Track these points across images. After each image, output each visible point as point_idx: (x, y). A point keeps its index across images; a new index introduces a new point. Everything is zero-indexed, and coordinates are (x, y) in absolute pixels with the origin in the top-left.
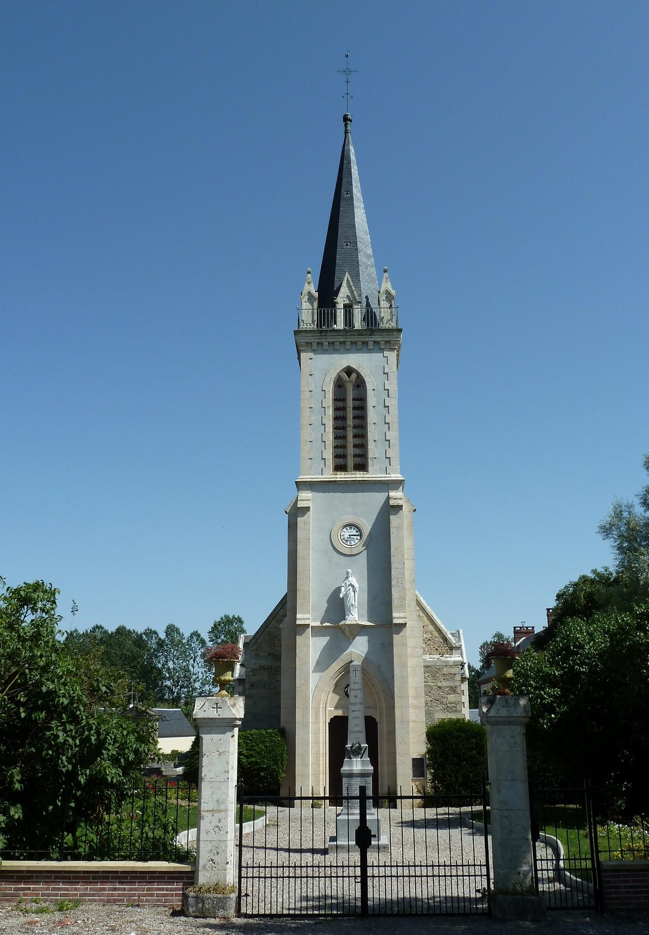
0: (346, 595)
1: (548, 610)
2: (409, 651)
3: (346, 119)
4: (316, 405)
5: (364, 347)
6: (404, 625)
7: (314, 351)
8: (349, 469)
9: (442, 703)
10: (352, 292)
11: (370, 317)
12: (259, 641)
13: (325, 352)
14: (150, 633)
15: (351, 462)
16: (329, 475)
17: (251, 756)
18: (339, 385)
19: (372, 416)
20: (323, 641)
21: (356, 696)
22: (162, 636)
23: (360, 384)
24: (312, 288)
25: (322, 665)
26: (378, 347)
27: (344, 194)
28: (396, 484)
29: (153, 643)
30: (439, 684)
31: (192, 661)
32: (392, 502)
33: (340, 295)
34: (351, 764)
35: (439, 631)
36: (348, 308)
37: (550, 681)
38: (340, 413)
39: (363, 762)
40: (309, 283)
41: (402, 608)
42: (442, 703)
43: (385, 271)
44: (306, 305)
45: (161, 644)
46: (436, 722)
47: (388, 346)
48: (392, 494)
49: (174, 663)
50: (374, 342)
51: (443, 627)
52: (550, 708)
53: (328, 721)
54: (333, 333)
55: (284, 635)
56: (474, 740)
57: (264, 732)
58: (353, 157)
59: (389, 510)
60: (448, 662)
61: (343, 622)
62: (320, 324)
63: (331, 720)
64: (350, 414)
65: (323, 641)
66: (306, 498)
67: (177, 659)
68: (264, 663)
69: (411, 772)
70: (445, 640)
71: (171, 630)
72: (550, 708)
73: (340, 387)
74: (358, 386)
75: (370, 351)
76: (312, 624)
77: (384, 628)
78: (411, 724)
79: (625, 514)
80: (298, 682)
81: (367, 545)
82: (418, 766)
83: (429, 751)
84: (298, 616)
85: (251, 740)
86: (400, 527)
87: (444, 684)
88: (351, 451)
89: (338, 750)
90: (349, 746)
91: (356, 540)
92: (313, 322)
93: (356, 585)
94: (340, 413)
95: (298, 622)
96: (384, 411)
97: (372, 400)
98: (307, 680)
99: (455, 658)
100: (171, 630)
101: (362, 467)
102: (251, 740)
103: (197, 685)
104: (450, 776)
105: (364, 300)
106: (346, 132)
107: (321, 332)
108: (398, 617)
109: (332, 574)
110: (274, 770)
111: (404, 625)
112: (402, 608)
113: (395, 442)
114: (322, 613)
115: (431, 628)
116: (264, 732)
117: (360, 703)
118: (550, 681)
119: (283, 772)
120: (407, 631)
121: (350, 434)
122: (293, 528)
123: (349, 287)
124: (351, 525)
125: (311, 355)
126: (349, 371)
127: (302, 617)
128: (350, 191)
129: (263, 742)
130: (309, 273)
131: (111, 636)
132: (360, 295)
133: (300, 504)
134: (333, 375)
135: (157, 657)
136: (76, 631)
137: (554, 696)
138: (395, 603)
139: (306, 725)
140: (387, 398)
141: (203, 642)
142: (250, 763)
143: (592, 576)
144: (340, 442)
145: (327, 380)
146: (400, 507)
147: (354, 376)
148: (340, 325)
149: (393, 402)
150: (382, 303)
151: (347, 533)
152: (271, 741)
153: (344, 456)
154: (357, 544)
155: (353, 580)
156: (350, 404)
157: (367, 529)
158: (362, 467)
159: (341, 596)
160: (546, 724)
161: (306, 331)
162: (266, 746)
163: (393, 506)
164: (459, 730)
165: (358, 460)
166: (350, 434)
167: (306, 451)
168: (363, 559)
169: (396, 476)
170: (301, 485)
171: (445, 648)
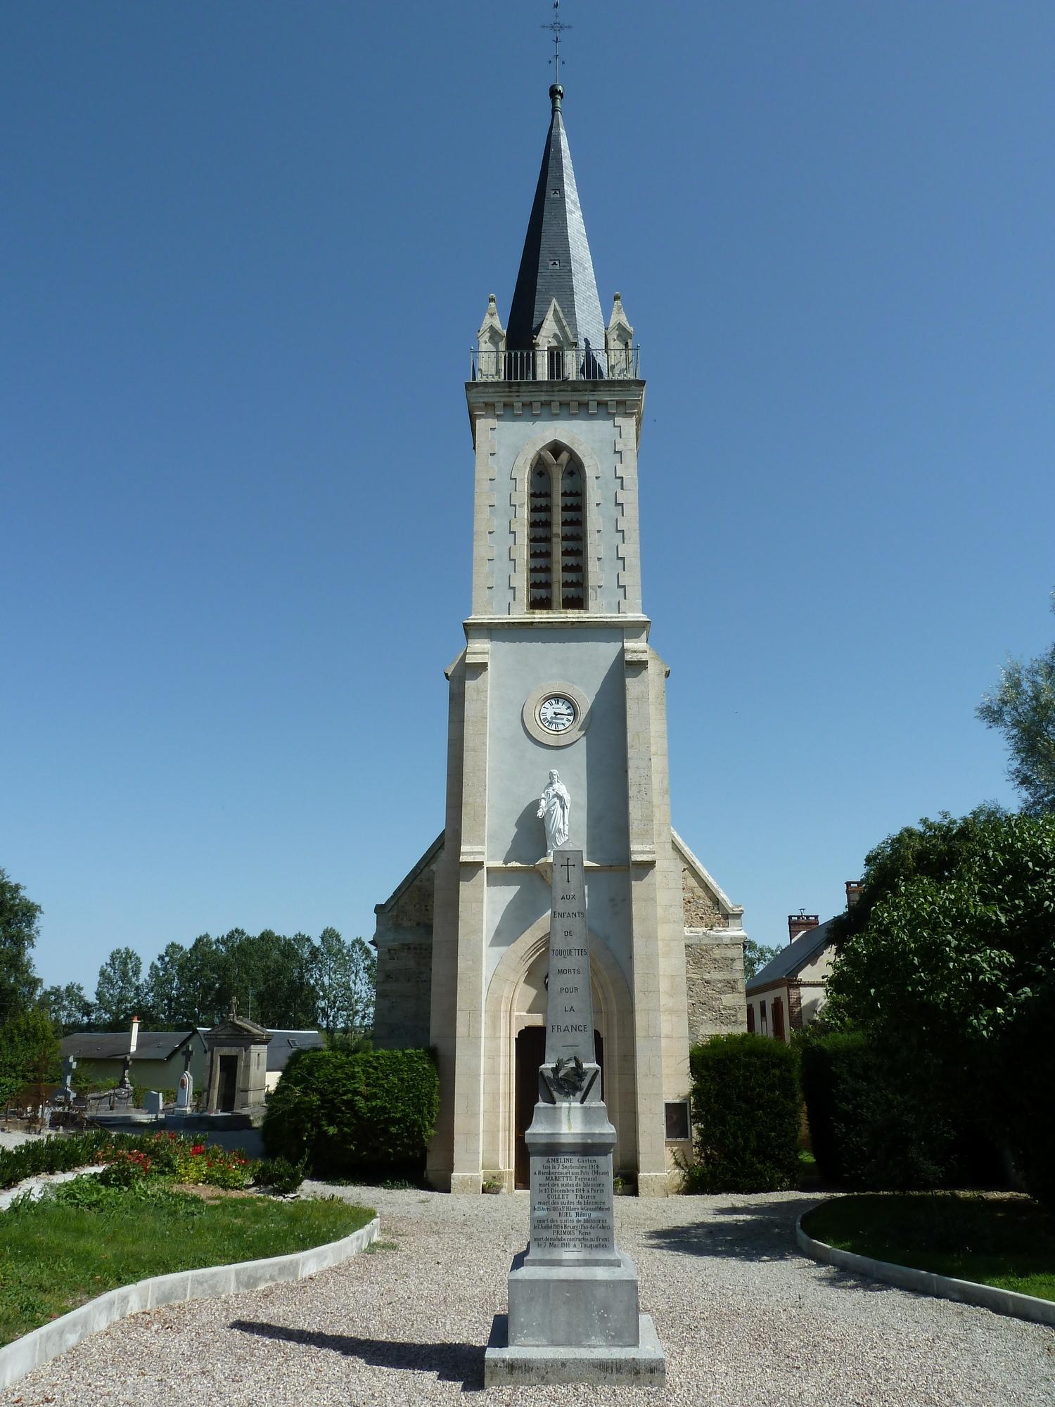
0: (549, 813)
1: (848, 884)
2: (660, 911)
3: (554, 92)
4: (499, 500)
5: (582, 410)
6: (651, 865)
7: (499, 417)
8: (555, 604)
9: (711, 1009)
10: (562, 328)
11: (590, 366)
12: (401, 903)
13: (516, 418)
14: (303, 939)
15: (558, 593)
16: (521, 613)
17: (374, 1096)
18: (540, 470)
19: (595, 519)
20: (508, 893)
21: (568, 933)
22: (317, 942)
23: (575, 469)
24: (496, 320)
25: (505, 935)
26: (604, 411)
27: (550, 194)
28: (635, 629)
29: (306, 953)
30: (707, 976)
31: (353, 976)
32: (628, 657)
33: (543, 332)
34: (553, 1118)
35: (706, 887)
36: (556, 358)
37: (987, 934)
38: (542, 516)
39: (588, 1114)
40: (492, 315)
41: (647, 835)
42: (711, 1009)
43: (617, 298)
44: (485, 345)
45: (315, 952)
46: (703, 1041)
47: (621, 409)
48: (629, 645)
49: (330, 978)
50: (599, 403)
51: (711, 880)
52: (991, 995)
53: (515, 1035)
54: (531, 388)
55: (438, 883)
56: (777, 1072)
57: (400, 1054)
58: (567, 161)
59: (626, 668)
60: (721, 938)
61: (543, 860)
62: (508, 374)
63: (521, 1033)
64: (558, 517)
65: (508, 893)
66: (480, 649)
67: (335, 973)
68: (409, 938)
69: (664, 1131)
70: (716, 902)
71: (330, 936)
72: (991, 995)
73: (540, 474)
74: (571, 473)
75: (592, 417)
76: (487, 864)
77: (618, 868)
78: (664, 1042)
79: (1026, 685)
80: (462, 964)
81: (588, 728)
82: (677, 1118)
83: (695, 1091)
84: (464, 848)
85: (375, 1068)
86: (642, 698)
87: (715, 975)
88: (558, 576)
89: (534, 1084)
90: (548, 1065)
91: (566, 721)
92: (498, 372)
93: (567, 797)
94: (542, 516)
95: (463, 859)
96: (615, 511)
97: (594, 494)
98: (477, 960)
99: (734, 932)
100: (330, 936)
101: (577, 602)
102: (375, 1068)
103: (359, 1007)
104: (735, 1137)
105: (582, 344)
106: (554, 110)
107: (510, 385)
108: (639, 850)
109: (523, 775)
110: (414, 1123)
111: (651, 865)
112: (647, 835)
113: (633, 560)
114: (507, 845)
115: (692, 882)
116: (400, 1054)
117: (582, 952)
118: (987, 934)
119: (432, 1126)
120: (657, 875)
121: (558, 548)
122: (457, 700)
123: (558, 321)
124: (557, 697)
125: (492, 422)
126: (556, 448)
127: (468, 851)
128: (560, 189)
129: (397, 1072)
130: (492, 300)
131: (251, 942)
132: (576, 336)
133: (470, 659)
134: (529, 455)
135: (309, 970)
136: (207, 936)
137: (1000, 966)
138: (635, 826)
139: (474, 1041)
140: (619, 491)
141: (367, 952)
142: (371, 1110)
143: (919, 828)
144: (540, 562)
145: (520, 461)
146: (642, 665)
147: (564, 456)
148: (543, 373)
149: (630, 498)
150: (612, 345)
151: (549, 710)
152: (411, 1070)
153: (547, 585)
154: (570, 730)
155: (560, 788)
156: (558, 500)
157: (585, 702)
158: (577, 602)
159: (540, 814)
160: (986, 1028)
161: (485, 384)
162: (402, 1080)
163: (630, 663)
164: (751, 1053)
165: (572, 591)
166: (558, 548)
167: (482, 575)
168: (579, 755)
169: (635, 615)
170: (471, 630)
171: (715, 916)
